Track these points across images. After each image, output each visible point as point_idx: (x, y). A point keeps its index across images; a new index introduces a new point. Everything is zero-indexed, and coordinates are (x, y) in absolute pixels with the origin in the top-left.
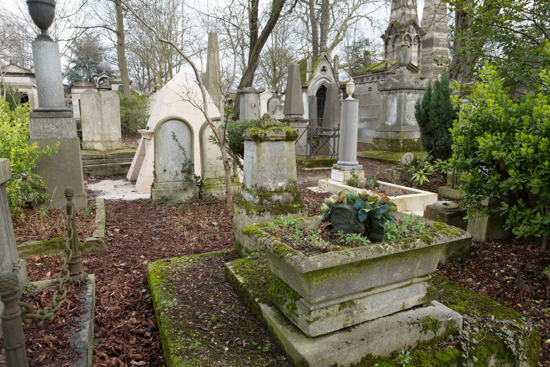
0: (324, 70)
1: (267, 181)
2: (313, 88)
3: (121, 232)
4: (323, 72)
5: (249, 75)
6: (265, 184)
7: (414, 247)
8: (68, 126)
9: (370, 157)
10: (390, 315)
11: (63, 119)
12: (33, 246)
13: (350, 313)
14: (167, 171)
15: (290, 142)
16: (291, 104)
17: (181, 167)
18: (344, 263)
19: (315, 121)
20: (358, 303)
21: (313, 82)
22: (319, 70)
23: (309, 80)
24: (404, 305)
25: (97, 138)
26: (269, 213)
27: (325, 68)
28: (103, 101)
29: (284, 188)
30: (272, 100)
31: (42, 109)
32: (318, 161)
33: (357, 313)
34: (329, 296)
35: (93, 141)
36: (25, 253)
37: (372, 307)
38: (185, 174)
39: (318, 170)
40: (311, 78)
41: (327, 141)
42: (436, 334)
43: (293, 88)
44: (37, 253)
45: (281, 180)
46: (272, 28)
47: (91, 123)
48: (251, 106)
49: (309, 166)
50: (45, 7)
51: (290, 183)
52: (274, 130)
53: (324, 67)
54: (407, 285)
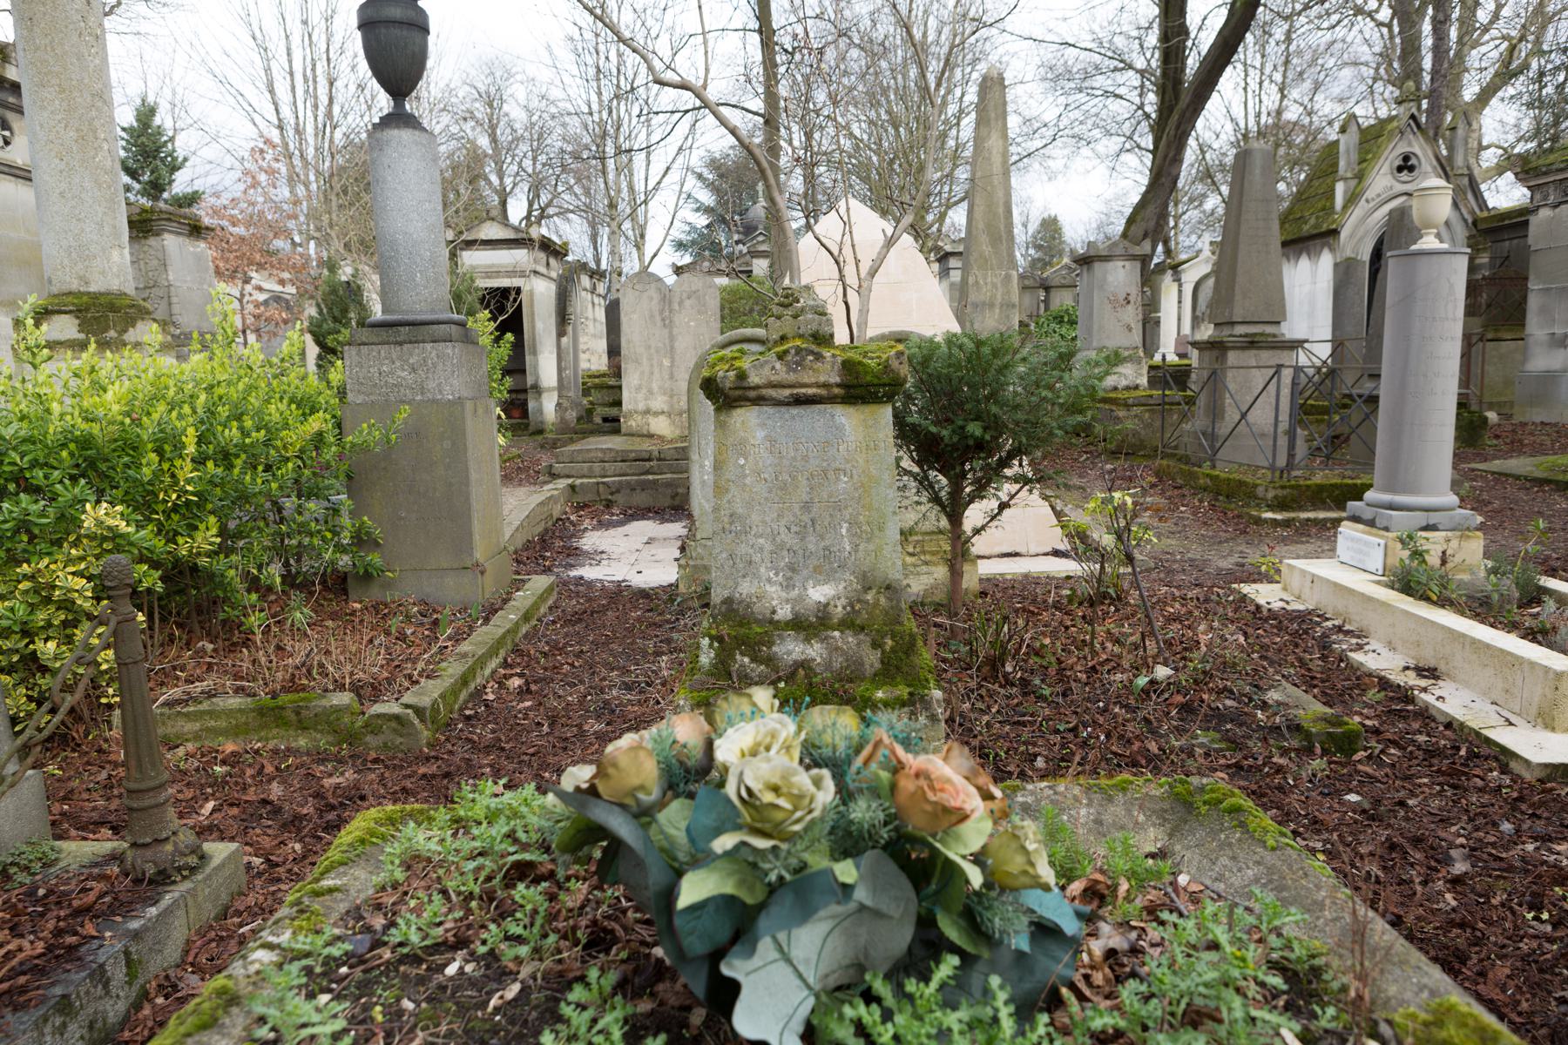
1: (756, 576)
3: (524, 692)
4: (1404, 176)
5: (1151, 210)
6: (746, 588)
11: (428, 346)
12: (229, 713)
15: (868, 410)
22: (1386, 168)
23: (1345, 207)
25: (659, 403)
27: (1413, 161)
28: (676, 300)
29: (839, 611)
31: (389, 317)
32: (1321, 488)
35: (647, 412)
36: (208, 730)
39: (1316, 522)
40: (1352, 199)
41: (1367, 416)
44: (237, 735)
45: (823, 573)
46: (1234, 51)
49: (1281, 505)
50: (396, 32)
51: (867, 589)
52: (781, 357)
53: (1406, 158)
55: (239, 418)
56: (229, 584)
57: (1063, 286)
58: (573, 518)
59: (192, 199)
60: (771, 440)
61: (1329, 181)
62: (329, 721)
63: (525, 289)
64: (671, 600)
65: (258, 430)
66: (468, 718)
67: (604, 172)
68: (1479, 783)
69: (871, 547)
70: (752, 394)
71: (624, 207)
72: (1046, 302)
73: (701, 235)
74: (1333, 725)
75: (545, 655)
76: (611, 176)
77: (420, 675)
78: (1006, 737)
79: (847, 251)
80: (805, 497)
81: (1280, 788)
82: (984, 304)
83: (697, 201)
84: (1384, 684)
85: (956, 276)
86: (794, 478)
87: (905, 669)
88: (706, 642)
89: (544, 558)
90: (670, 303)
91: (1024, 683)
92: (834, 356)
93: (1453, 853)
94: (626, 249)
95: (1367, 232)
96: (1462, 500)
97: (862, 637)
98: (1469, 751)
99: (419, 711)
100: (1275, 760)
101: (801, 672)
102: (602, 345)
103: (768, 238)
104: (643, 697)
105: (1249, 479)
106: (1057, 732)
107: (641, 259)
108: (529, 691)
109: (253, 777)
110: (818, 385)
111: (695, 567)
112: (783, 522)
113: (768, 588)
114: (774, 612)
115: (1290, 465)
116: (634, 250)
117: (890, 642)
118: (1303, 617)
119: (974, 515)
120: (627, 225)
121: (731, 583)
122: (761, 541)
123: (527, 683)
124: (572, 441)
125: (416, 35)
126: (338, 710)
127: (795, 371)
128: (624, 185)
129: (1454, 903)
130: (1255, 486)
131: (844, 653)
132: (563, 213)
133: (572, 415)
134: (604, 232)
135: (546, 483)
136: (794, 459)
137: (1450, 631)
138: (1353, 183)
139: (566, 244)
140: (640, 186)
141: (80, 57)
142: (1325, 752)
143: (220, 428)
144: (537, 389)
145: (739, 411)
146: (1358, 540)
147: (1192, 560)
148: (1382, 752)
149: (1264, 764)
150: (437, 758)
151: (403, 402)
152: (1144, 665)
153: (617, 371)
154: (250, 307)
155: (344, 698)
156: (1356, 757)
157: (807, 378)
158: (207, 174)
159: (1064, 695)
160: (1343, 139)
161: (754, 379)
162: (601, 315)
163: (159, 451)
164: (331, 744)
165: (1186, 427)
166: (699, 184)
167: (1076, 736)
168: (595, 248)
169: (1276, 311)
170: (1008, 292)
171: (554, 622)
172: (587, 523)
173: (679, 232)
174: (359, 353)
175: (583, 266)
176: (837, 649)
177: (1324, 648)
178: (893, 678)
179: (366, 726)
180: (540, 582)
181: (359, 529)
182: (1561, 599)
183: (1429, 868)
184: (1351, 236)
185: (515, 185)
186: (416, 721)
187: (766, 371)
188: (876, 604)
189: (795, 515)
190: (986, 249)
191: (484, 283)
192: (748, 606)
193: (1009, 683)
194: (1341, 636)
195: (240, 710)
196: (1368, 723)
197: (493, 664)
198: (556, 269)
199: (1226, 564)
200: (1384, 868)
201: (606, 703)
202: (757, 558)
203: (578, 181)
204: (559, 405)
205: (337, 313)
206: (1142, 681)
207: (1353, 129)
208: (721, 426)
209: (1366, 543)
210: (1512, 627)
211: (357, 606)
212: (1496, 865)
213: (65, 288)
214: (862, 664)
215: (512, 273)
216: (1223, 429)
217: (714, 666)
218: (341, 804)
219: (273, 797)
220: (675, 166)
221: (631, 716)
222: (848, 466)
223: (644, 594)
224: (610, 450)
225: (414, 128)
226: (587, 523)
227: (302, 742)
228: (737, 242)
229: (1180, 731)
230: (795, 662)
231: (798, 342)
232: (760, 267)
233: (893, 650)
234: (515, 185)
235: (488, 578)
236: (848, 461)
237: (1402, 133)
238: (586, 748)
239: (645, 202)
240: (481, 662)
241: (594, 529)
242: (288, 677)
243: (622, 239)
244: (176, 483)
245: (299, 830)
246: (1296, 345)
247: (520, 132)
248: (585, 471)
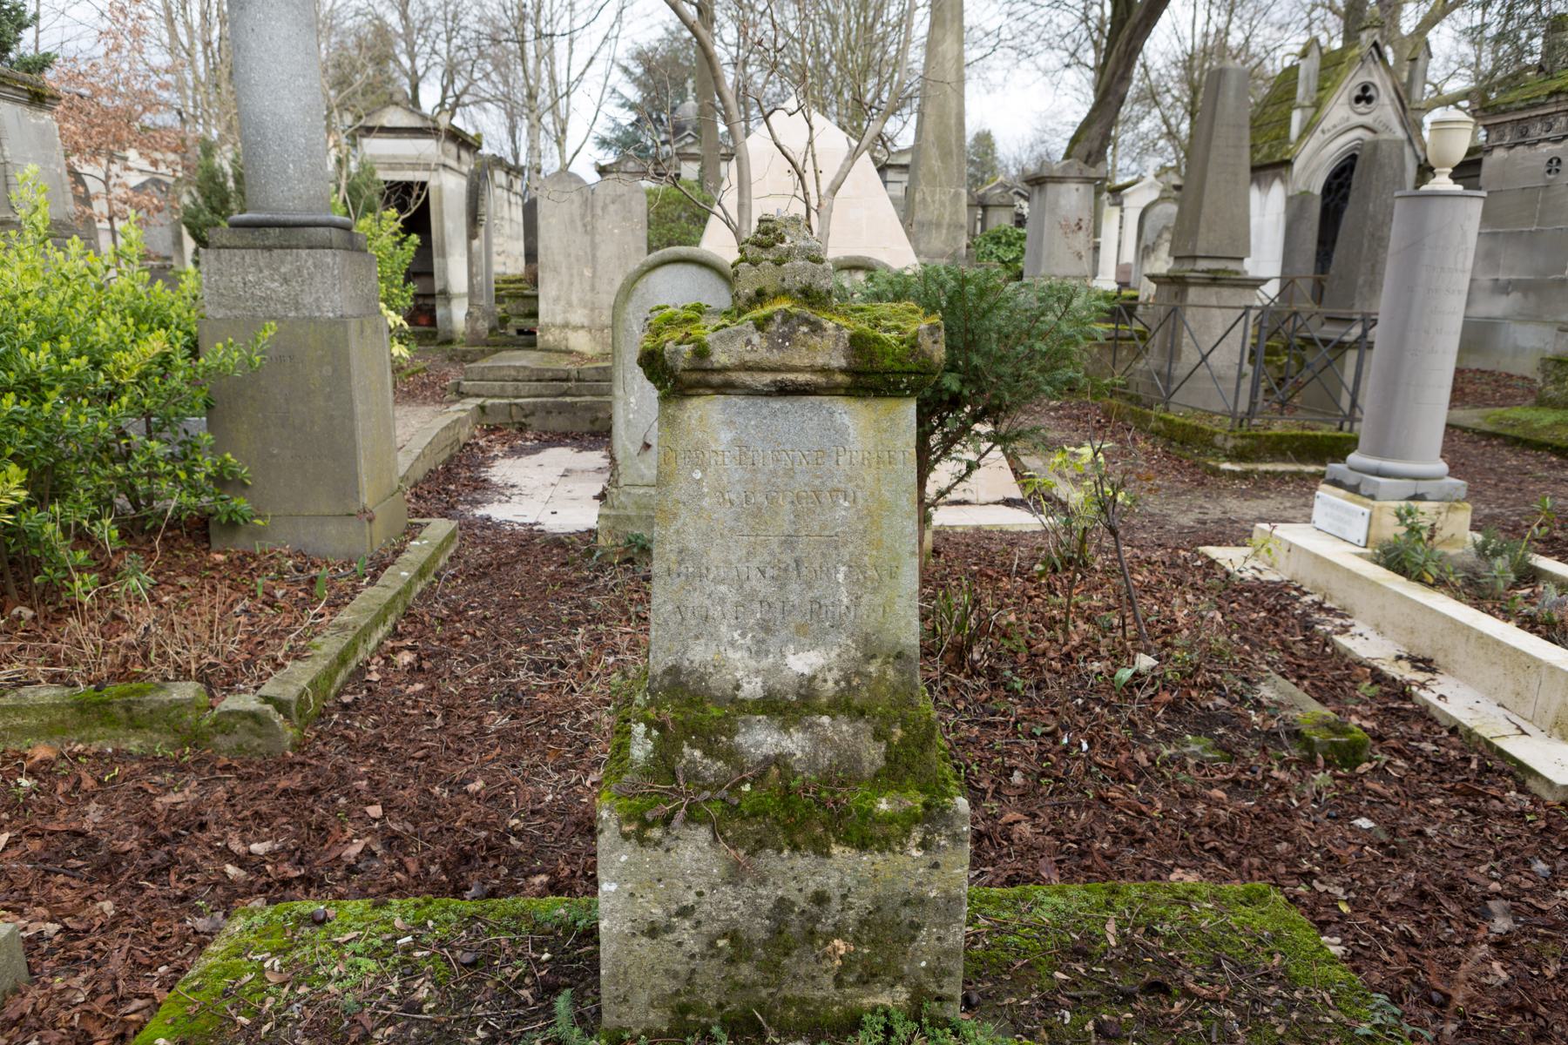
0: (1365, 96)
2: (1314, 164)
3: (415, 670)
4: (1362, 107)
5: (1096, 130)
6: (699, 654)
8: (318, 278)
9: (1516, 432)
11: (304, 253)
12: (39, 709)
14: (655, 448)
15: (883, 406)
16: (1198, 221)
19: (1305, 287)
21: (1312, 143)
22: (1344, 99)
23: (1301, 137)
25: (578, 316)
26: (703, 834)
27: (1372, 92)
28: (599, 204)
29: (829, 688)
30: (1158, 209)
32: (1281, 439)
35: (566, 326)
36: (14, 729)
40: (1308, 129)
41: (1329, 363)
43: (1213, 155)
44: (51, 735)
45: (810, 633)
47: (564, 270)
48: (1065, 227)
49: (1239, 455)
52: (761, 325)
53: (1365, 88)
55: (54, 338)
56: (48, 540)
57: (1001, 205)
58: (482, 443)
59: (43, 63)
60: (742, 446)
61: (1284, 108)
62: (169, 717)
63: (433, 183)
64: (590, 553)
65: (78, 357)
66: (346, 706)
67: (523, 59)
68: (1499, 806)
69: (878, 600)
70: (716, 379)
71: (544, 98)
72: (984, 220)
73: (626, 133)
74: (1337, 733)
75: (442, 621)
76: (531, 64)
77: (286, 656)
78: (975, 742)
79: (809, 166)
80: (787, 528)
81: (1285, 811)
82: (931, 223)
83: (622, 96)
84: (1378, 677)
85: (899, 191)
86: (772, 501)
87: (918, 768)
88: (640, 729)
89: (447, 492)
90: (593, 207)
91: (993, 672)
92: (838, 327)
93: (1492, 905)
94: (545, 143)
95: (1320, 165)
96: (1451, 467)
97: (861, 724)
98: (1481, 764)
99: (281, 705)
100: (1275, 773)
101: (775, 771)
102: (519, 247)
103: (697, 141)
104: (554, 682)
105: (1207, 426)
106: (1033, 736)
107: (562, 156)
108: (421, 669)
109: (66, 795)
110: (813, 370)
111: (617, 517)
112: (755, 563)
113: (730, 653)
114: (738, 687)
115: (1250, 413)
116: (555, 147)
117: (898, 732)
118: (1279, 589)
119: (942, 474)
120: (547, 119)
121: (677, 646)
122: (723, 588)
123: (420, 659)
124: (484, 355)
126: (179, 705)
127: (780, 347)
128: (545, 75)
129: (1504, 976)
130: (1213, 434)
131: (835, 746)
132: (479, 102)
133: (483, 326)
134: (523, 126)
135: (453, 402)
136: (774, 473)
137: (1453, 622)
138: (1311, 111)
139: (479, 136)
140: (561, 77)
142: (1329, 764)
143: (24, 351)
144: (446, 295)
145: (696, 402)
146: (1339, 507)
147: (1151, 515)
148: (1388, 763)
149: (1264, 780)
150: (303, 764)
151: (272, 318)
152: (1121, 656)
153: (533, 280)
154: (119, 192)
155: (187, 690)
156: (1362, 769)
157: (799, 358)
158: (79, 37)
159: (1038, 688)
160: (1303, 64)
161: (720, 357)
162: (518, 214)
164: (172, 747)
165: (1141, 365)
166: (625, 78)
167: (1056, 742)
168: (514, 142)
169: (1240, 248)
170: (957, 212)
171: (455, 577)
172: (497, 449)
173: (603, 129)
174: (218, 258)
175: (498, 162)
176: (825, 740)
177: (1306, 628)
178: (901, 780)
179: (215, 724)
180: (440, 528)
181: (221, 467)
182: (1565, 586)
183: (1468, 925)
184: (1304, 168)
185: (428, 68)
186: (279, 719)
187: (739, 345)
188: (882, 677)
189: (772, 554)
190: (936, 164)
191: (384, 175)
192: (701, 678)
193: (975, 672)
194: (1323, 616)
195: (54, 706)
196: (1367, 724)
197: (379, 634)
198: (468, 162)
199: (1188, 520)
200: (1418, 924)
201: (512, 688)
202: (716, 612)
203: (496, 68)
204: (469, 314)
205: (215, 203)
206: (1125, 674)
207: (1315, 54)
208: (668, 422)
209: (1348, 511)
210: (1506, 615)
211: (220, 558)
212: (1538, 920)
214: (859, 761)
215: (414, 166)
216: (1181, 370)
217: (653, 762)
218: (176, 835)
219: (87, 826)
220: (599, 56)
221: (540, 709)
222: (851, 485)
223: (559, 542)
224: (525, 368)
226: (497, 449)
227: (134, 744)
228: (663, 143)
229: (1166, 736)
230: (767, 758)
231: (785, 305)
232: (690, 171)
234: (428, 68)
235: (378, 527)
236: (850, 479)
237: (1363, 61)
238: (487, 752)
239: (567, 94)
240: (364, 634)
241: (505, 456)
242: (118, 661)
243: (542, 133)
245: (114, 880)
246: (1257, 283)
247: (432, 11)
248: (497, 391)
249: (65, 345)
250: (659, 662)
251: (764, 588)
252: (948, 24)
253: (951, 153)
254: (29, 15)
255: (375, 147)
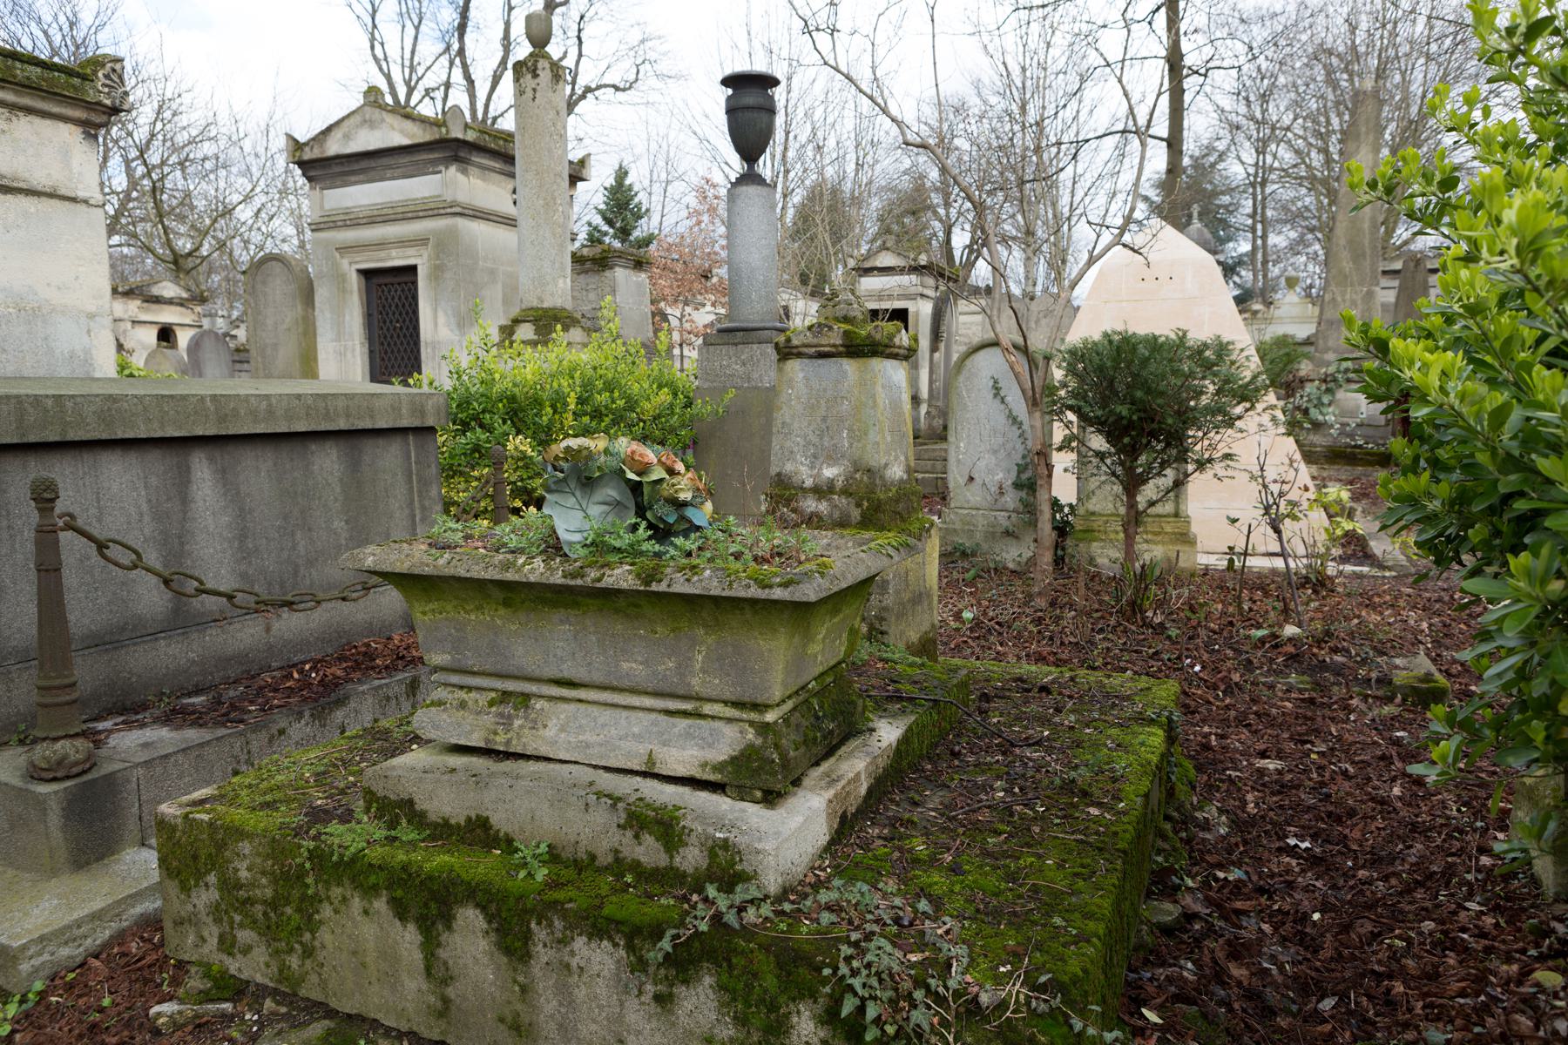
1: (795, 460)
6: (789, 467)
7: (599, 580)
8: (762, 362)
10: (607, 769)
11: (755, 346)
13: (507, 722)
15: (861, 361)
17: (1014, 474)
18: (416, 571)
20: (538, 706)
24: (651, 760)
28: (1033, 318)
29: (839, 484)
33: (521, 727)
34: (459, 660)
37: (562, 729)
38: (1023, 494)
42: (672, 857)
45: (832, 460)
54: (685, 714)
59: (647, 241)
60: (806, 378)
63: (911, 310)
70: (795, 351)
80: (824, 414)
125: (764, 116)
141: (550, 151)
163: (553, 406)
170: (1369, 309)
188: (861, 481)
202: (796, 449)
213: (530, 305)
225: (759, 184)
233: (868, 509)
244: (563, 428)
248: (929, 468)
249: (616, 394)
250: (774, 470)
251: (814, 439)
252: (1363, 137)
253: (1364, 255)
254: (643, 210)
255: (869, 283)
